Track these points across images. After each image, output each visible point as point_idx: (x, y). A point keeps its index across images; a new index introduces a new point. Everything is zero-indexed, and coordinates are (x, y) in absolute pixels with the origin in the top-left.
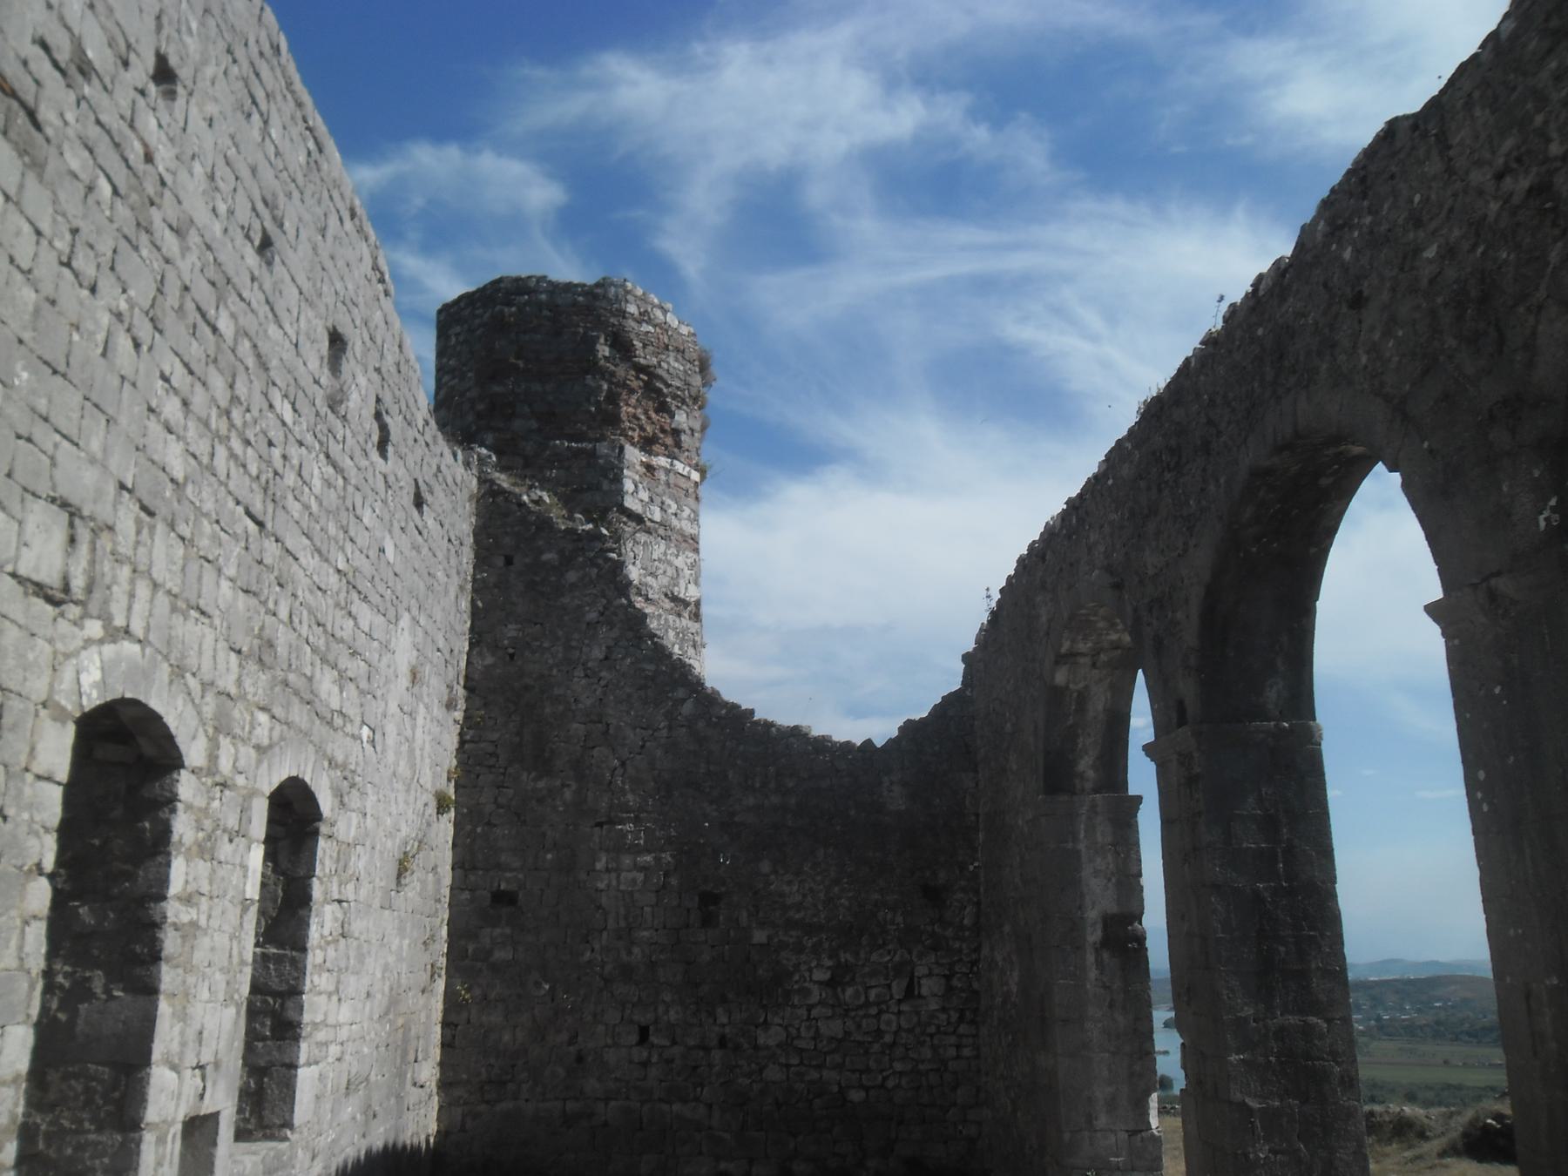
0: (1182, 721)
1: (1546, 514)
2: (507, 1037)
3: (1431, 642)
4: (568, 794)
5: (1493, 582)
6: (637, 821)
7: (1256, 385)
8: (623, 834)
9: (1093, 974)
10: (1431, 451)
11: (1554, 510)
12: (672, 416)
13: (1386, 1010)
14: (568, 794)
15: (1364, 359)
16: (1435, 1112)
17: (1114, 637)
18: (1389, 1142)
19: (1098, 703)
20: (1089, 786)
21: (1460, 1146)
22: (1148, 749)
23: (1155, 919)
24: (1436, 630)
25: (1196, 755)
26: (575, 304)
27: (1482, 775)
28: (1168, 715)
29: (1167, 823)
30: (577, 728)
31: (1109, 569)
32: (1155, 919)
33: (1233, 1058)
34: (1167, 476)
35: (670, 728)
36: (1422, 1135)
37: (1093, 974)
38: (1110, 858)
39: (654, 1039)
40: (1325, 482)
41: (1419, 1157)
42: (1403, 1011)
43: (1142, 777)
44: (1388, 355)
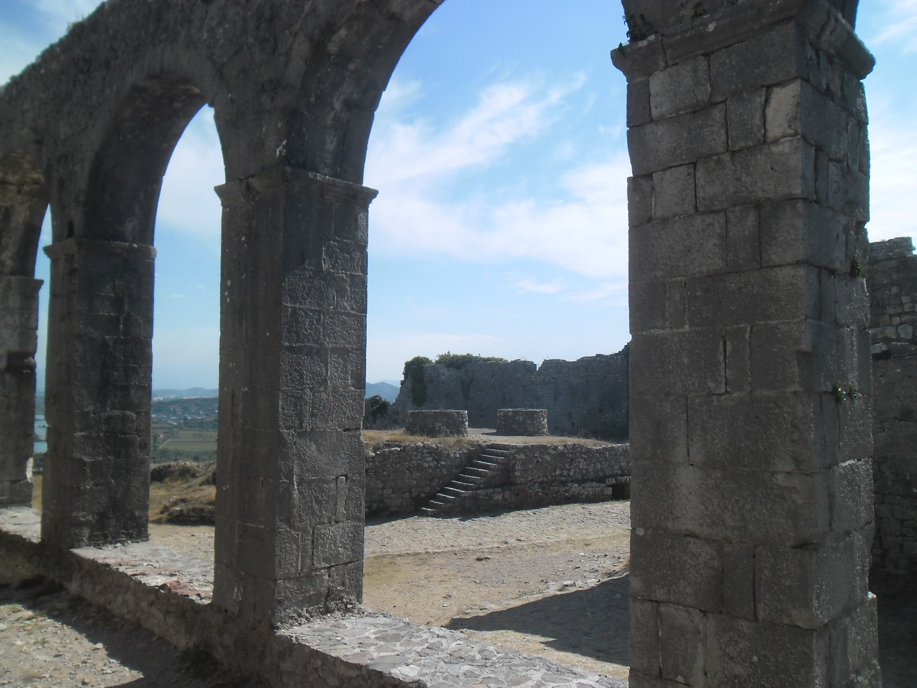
0: (71, 234)
1: (280, 148)
3: (214, 210)
5: (250, 180)
7: (143, 33)
10: (232, 100)
11: (284, 147)
13: (190, 414)
15: (205, 35)
16: (202, 464)
17: (35, 176)
18: (176, 480)
19: (20, 217)
20: (7, 270)
21: (211, 479)
22: (47, 250)
23: (41, 359)
24: (218, 201)
25: (77, 256)
27: (229, 283)
28: (62, 231)
29: (54, 296)
31: (34, 129)
32: (41, 359)
33: (78, 434)
34: (81, 77)
36: (194, 476)
38: (17, 317)
40: (177, 105)
41: (189, 487)
42: (199, 414)
43: (43, 268)
44: (218, 37)
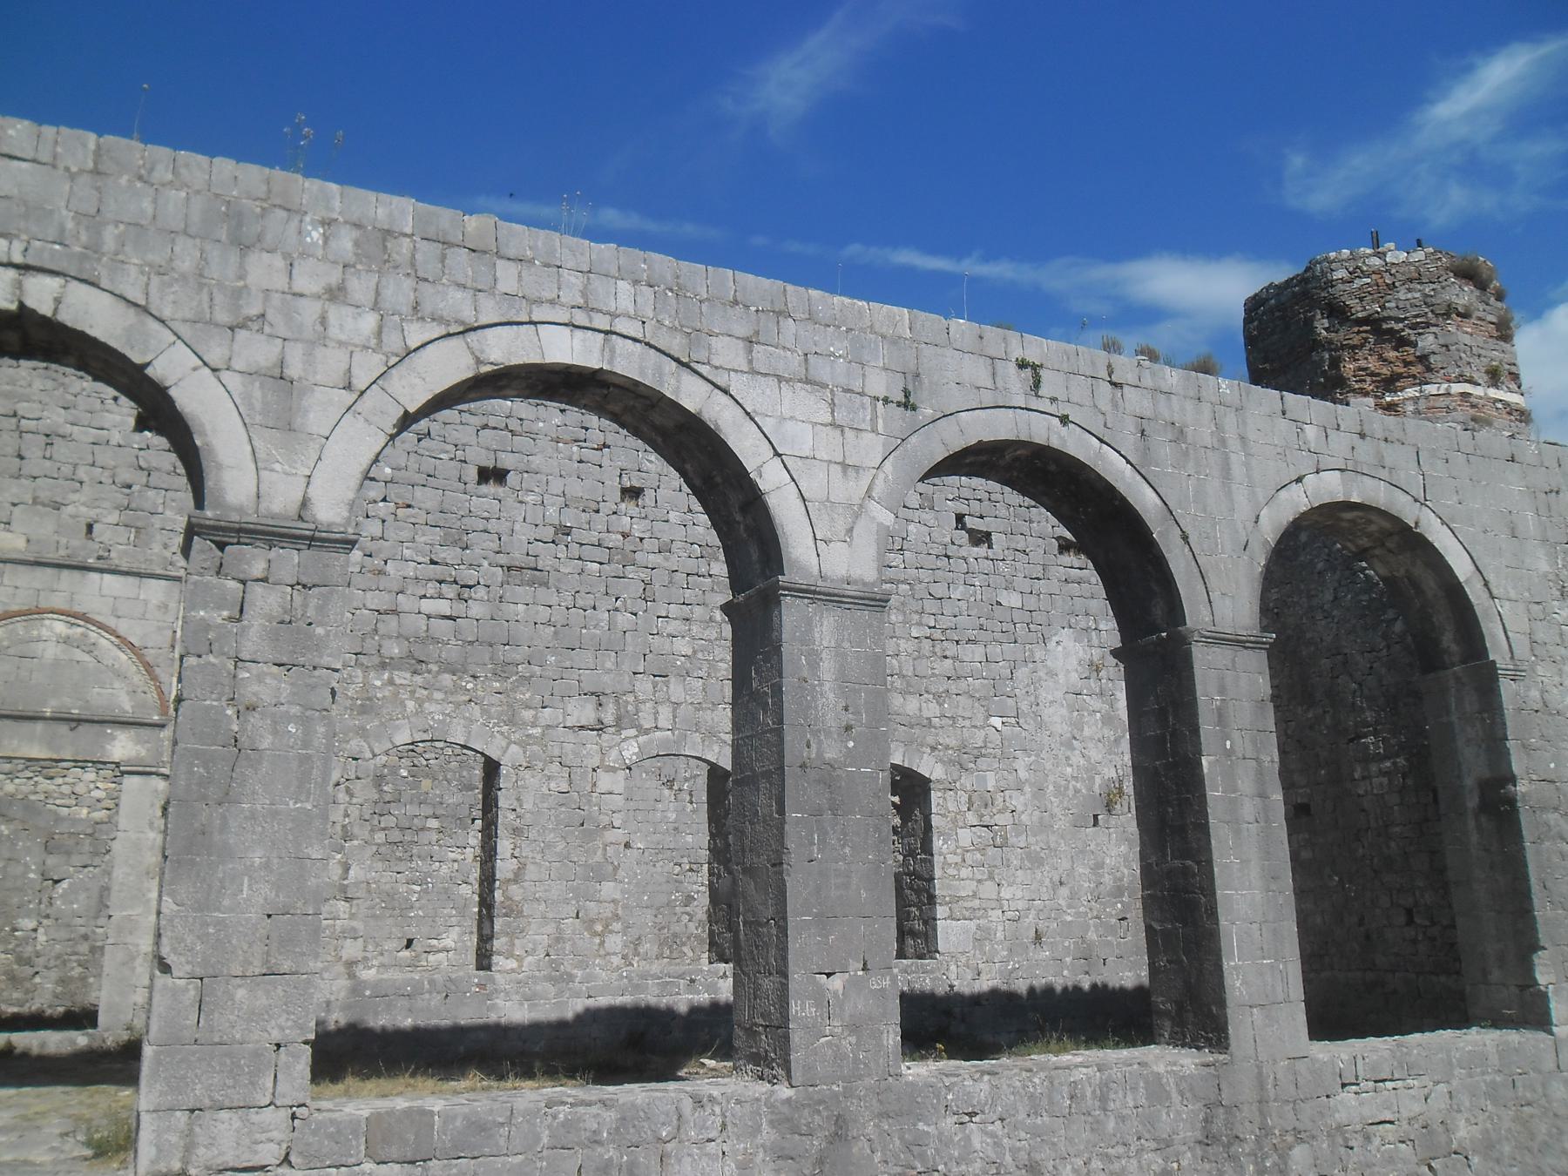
2: (1319, 920)
4: (1328, 720)
6: (1375, 733)
8: (1366, 746)
9: (1474, 838)
12: (1415, 345)
14: (1328, 720)
20: (1456, 659)
26: (1294, 294)
30: (1325, 663)
35: (1388, 647)
37: (1474, 838)
39: (1418, 920)
